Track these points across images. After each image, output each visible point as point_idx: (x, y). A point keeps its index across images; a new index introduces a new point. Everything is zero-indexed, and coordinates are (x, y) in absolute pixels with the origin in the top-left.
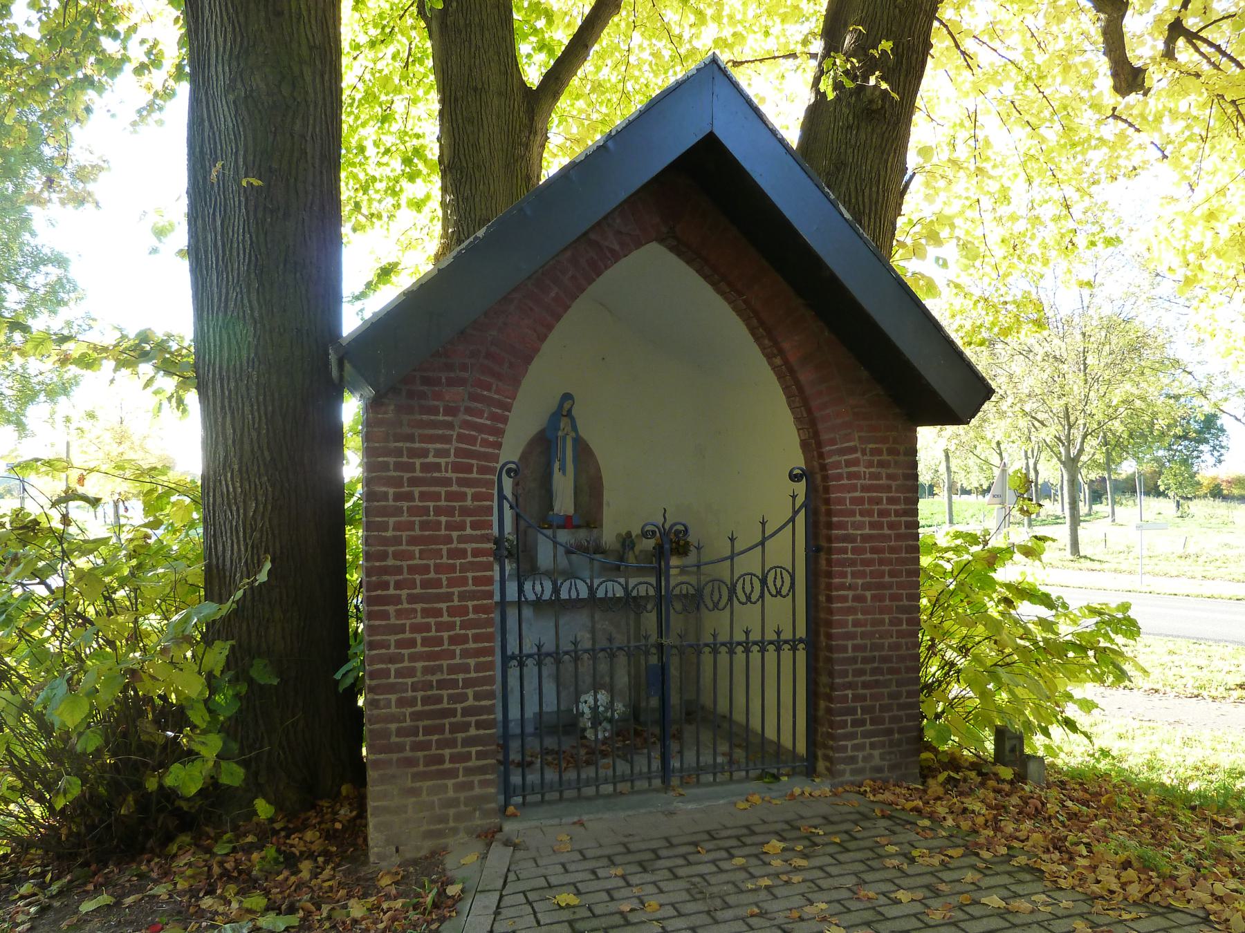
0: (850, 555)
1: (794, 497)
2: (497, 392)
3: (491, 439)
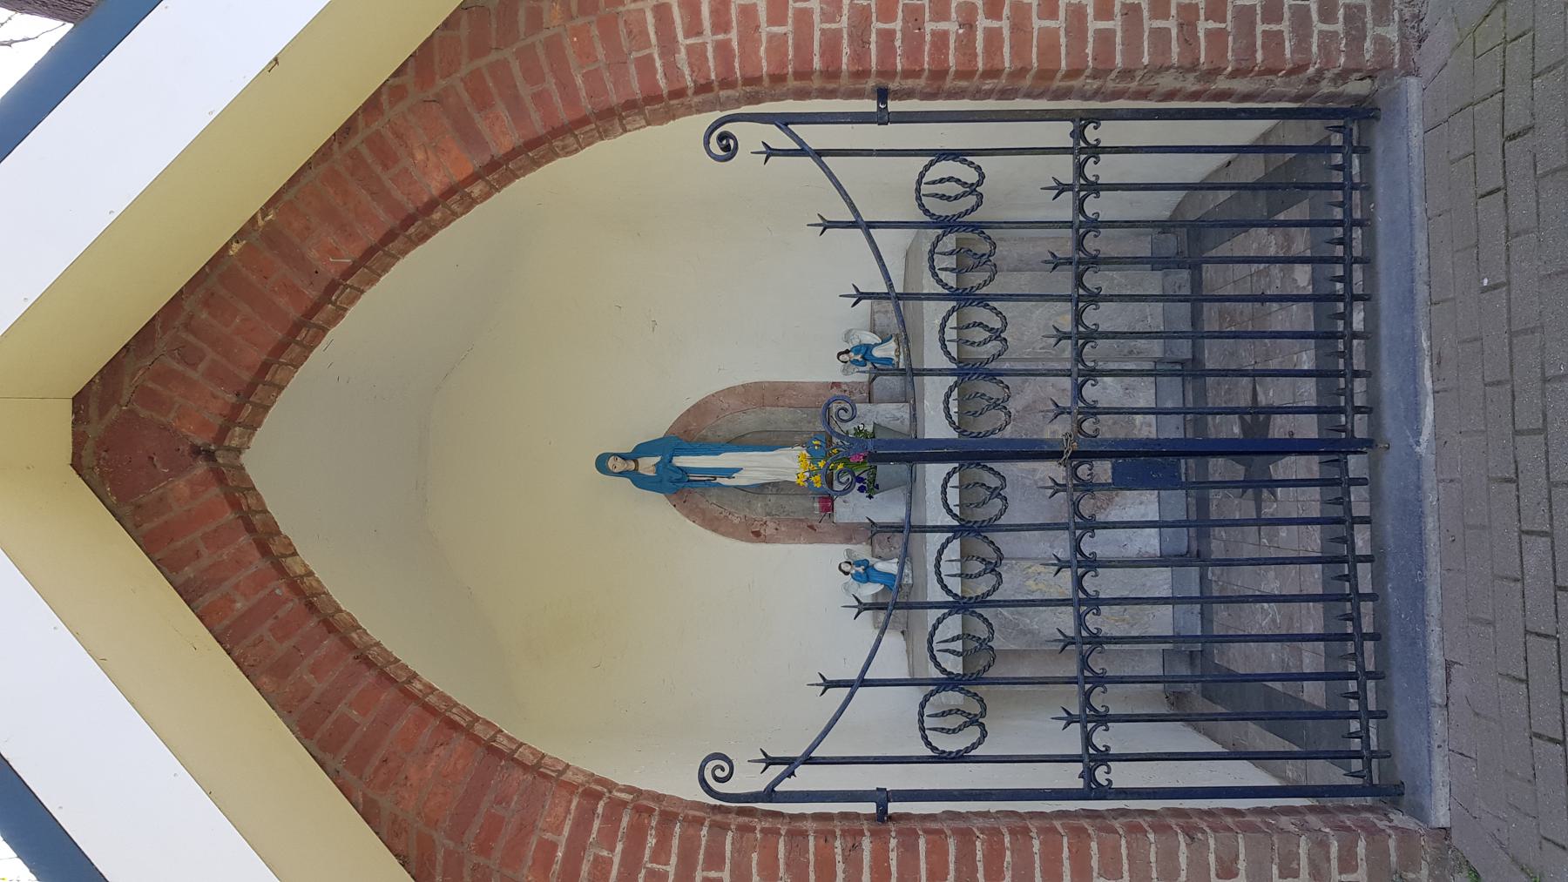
0: (897, 25)
1: (770, 152)
2: (558, 830)
3: (652, 841)
